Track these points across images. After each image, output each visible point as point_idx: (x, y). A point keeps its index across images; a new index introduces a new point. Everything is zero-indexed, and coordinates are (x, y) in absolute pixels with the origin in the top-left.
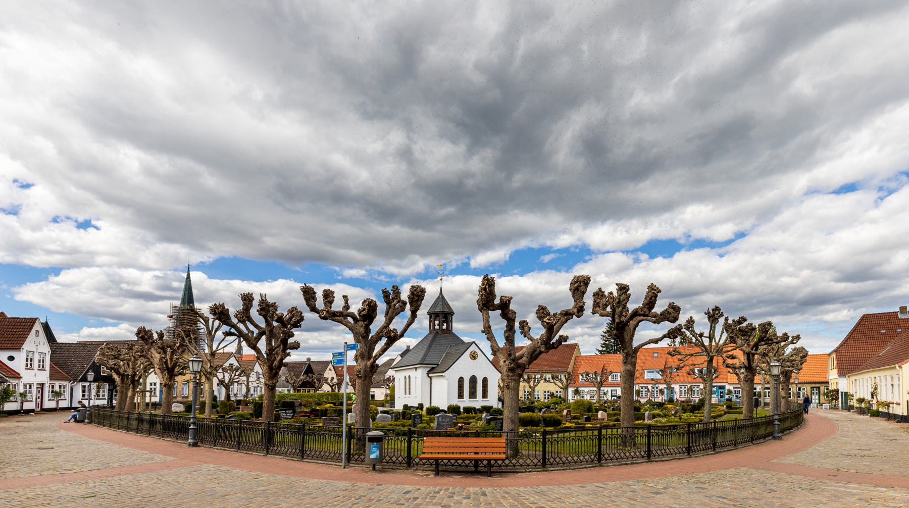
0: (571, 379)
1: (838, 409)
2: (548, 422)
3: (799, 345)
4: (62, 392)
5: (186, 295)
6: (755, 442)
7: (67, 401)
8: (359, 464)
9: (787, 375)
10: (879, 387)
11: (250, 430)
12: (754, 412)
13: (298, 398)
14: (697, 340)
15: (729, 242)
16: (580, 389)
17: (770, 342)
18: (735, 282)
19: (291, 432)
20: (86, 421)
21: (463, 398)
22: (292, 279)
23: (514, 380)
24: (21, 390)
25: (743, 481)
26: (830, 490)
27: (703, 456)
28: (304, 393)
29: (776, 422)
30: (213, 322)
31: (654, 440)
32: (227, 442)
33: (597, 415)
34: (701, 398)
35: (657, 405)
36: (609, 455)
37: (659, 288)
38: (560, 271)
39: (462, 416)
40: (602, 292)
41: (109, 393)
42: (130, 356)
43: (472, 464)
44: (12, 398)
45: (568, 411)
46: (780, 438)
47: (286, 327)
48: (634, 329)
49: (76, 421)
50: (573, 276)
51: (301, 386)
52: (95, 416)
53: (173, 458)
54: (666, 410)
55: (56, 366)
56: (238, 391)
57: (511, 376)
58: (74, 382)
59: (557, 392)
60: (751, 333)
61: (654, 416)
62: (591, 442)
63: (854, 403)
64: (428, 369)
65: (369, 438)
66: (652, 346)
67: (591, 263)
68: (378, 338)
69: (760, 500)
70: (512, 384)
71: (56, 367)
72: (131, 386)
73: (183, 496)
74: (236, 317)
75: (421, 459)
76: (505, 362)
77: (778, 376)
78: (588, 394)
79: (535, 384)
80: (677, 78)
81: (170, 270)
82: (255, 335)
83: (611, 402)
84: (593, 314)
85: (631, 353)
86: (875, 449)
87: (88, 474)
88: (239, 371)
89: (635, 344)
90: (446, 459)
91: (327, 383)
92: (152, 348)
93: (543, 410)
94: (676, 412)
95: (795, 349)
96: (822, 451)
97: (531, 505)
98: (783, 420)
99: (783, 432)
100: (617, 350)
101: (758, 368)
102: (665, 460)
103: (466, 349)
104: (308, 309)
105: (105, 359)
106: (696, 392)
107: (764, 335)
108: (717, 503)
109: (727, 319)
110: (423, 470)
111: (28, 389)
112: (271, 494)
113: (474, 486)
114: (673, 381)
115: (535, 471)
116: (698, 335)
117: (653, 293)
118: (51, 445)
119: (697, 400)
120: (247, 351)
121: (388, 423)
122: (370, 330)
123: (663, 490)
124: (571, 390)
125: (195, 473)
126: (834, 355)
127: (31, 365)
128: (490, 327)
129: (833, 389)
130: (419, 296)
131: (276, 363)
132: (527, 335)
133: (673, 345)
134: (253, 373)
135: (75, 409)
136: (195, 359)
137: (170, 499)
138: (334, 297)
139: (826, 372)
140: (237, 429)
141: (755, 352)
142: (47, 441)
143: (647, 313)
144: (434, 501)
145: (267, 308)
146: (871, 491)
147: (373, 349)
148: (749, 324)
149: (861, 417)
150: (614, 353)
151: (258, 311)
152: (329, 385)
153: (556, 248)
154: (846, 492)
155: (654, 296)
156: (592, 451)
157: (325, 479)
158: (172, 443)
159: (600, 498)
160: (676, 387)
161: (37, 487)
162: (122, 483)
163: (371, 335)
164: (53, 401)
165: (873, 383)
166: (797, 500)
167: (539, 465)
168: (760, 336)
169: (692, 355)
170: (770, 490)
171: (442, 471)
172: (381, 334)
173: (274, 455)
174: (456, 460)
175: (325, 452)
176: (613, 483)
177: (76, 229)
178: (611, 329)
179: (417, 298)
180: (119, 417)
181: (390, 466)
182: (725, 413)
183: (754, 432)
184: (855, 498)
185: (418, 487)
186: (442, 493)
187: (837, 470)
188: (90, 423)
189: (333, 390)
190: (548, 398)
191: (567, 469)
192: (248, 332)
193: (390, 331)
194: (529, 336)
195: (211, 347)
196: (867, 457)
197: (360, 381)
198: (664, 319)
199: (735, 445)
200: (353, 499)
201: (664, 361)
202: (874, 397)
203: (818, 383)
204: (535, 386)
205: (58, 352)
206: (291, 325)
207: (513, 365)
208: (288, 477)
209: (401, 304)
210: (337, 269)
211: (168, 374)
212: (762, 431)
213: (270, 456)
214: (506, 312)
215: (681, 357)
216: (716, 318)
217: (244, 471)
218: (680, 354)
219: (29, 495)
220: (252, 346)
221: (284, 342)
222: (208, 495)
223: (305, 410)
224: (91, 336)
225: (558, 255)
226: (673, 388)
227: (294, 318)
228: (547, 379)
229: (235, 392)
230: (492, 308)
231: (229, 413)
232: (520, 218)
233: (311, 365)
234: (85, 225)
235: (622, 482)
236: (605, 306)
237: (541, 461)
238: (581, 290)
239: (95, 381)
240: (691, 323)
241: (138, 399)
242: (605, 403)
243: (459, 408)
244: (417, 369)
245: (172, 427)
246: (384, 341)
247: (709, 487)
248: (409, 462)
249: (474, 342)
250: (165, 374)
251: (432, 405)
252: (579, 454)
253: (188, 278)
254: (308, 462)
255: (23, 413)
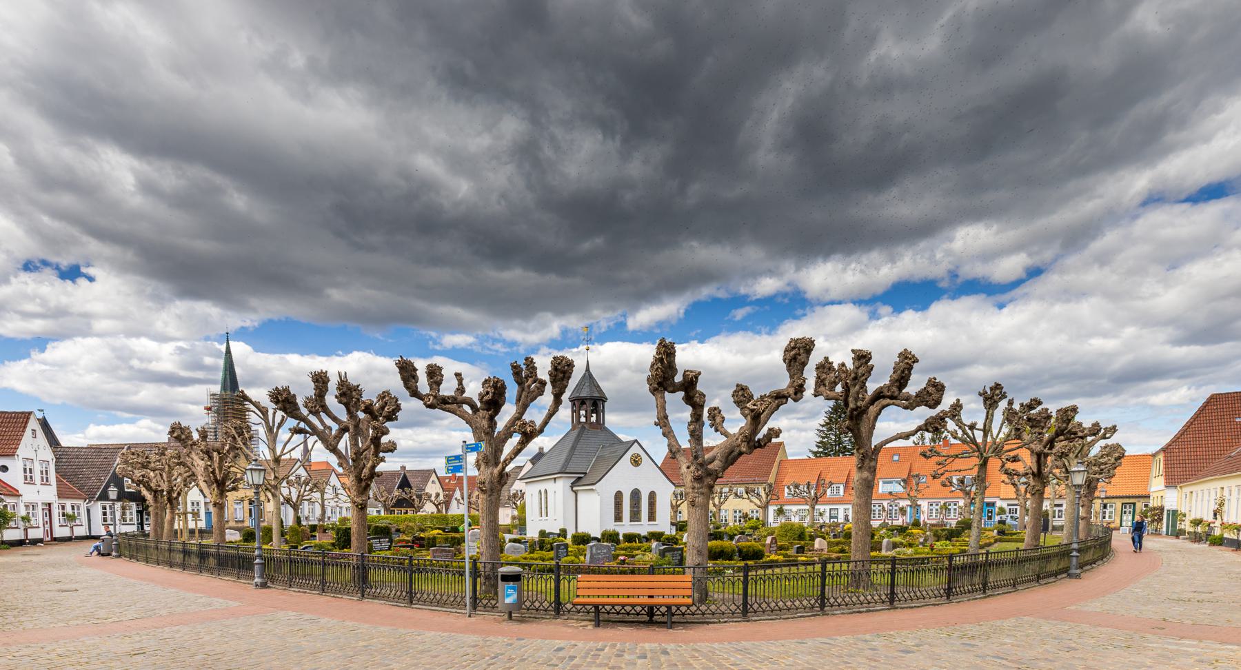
0: (772, 492)
1: (1161, 534)
2: (745, 555)
3: (1114, 440)
4: (76, 515)
5: (228, 376)
6: (1042, 581)
7: (84, 528)
8: (488, 611)
9: (1091, 486)
10: (1226, 503)
11: (337, 565)
12: (1042, 540)
13: (392, 522)
14: (964, 432)
15: (1017, 284)
16: (785, 508)
17: (1072, 436)
18: (1020, 345)
19: (393, 567)
20: (114, 553)
21: (655, 521)
22: (372, 351)
23: (702, 494)
24: (23, 512)
25: (1028, 636)
26: (1156, 648)
27: (968, 600)
28: (400, 515)
29: (1074, 553)
30: (274, 413)
31: (900, 579)
32: (307, 582)
33: (814, 544)
34: (960, 519)
35: (897, 529)
36: (836, 599)
37: (916, 356)
38: (759, 333)
39: (622, 545)
40: (830, 363)
41: (138, 516)
42: (162, 465)
43: (645, 611)
44: (12, 524)
45: (773, 539)
46: (1078, 576)
47: (378, 421)
48: (876, 418)
49: (100, 554)
50: (789, 340)
51: (395, 506)
52: (125, 547)
53: (238, 604)
54: (910, 536)
55: (64, 479)
56: (309, 512)
57: (698, 489)
58: (90, 501)
59: (752, 512)
60: (1045, 423)
61: (895, 546)
62: (811, 581)
63: (1187, 526)
64: (573, 480)
65: (502, 576)
66: (900, 443)
67: (805, 319)
68: (508, 434)
69: (1054, 661)
70: (699, 500)
71: (65, 481)
72: (168, 505)
73: (261, 653)
74: (306, 406)
75: (574, 605)
76: (688, 467)
77: (1079, 486)
78: (797, 514)
79: (722, 500)
80: (948, 15)
81: (199, 340)
82: (334, 432)
83: (830, 527)
84: (816, 396)
85: (870, 454)
86: (1218, 591)
87: (129, 624)
88: (310, 484)
89: (875, 442)
90: (609, 605)
91: (431, 501)
92: (193, 453)
93: (737, 537)
94: (926, 540)
95: (1105, 447)
96: (1140, 593)
97: (732, 667)
98: (1083, 550)
99: (1082, 568)
100: (839, 451)
101: (1051, 475)
102: (915, 607)
103: (624, 451)
104: (408, 393)
105: (129, 469)
106: (952, 511)
107: (1064, 425)
108: (993, 665)
109: (1011, 403)
110: (577, 620)
111: (31, 511)
112: (376, 651)
113: (650, 641)
114: (919, 496)
115: (733, 622)
116: (968, 426)
117: (907, 363)
118: (74, 586)
119: (954, 523)
120: (320, 454)
121: (521, 555)
122: (496, 424)
123: (915, 648)
124: (772, 509)
125: (270, 623)
126: (1161, 456)
127: (31, 477)
128: (666, 417)
129: (1156, 505)
130: (564, 372)
131: (366, 471)
132: (719, 428)
133: (921, 443)
134: (328, 487)
135: (97, 538)
136: (254, 467)
137: (244, 658)
138: (442, 376)
139: (1146, 480)
140: (320, 564)
141: (1049, 451)
142: (67, 581)
143: (896, 393)
144: (598, 661)
145: (348, 393)
146: (1215, 649)
147: (501, 451)
148: (1042, 409)
149: (1196, 545)
150: (834, 455)
151: (336, 397)
152: (434, 503)
153: (754, 298)
154: (1178, 650)
155: (908, 369)
156: (811, 594)
157: (445, 631)
158: (233, 583)
159: (827, 658)
160: (924, 504)
161: (68, 641)
162: (177, 636)
163: (497, 430)
164: (15, 530)
165: (1218, 496)
166: (1109, 662)
167: (738, 613)
168: (1059, 427)
169: (957, 456)
170: (1068, 648)
171: (603, 621)
172: (512, 429)
173: (371, 599)
174: (623, 606)
175: (442, 596)
176: (843, 638)
177: (59, 280)
178: (831, 420)
179: (561, 375)
180: (157, 548)
181: (532, 614)
182: (996, 541)
183: (1042, 568)
184: (1193, 660)
185: (573, 642)
186: (607, 649)
187: (1164, 620)
188: (119, 556)
189: (439, 511)
190: (740, 521)
191: (777, 619)
192: (324, 427)
193: (525, 424)
194: (722, 430)
195: (273, 450)
196: (1207, 603)
197: (485, 496)
198: (921, 403)
199: (1014, 586)
200: (487, 658)
201: (908, 467)
202: (1218, 516)
203: (1133, 497)
204: (721, 503)
205: (64, 460)
206: (384, 417)
207: (700, 472)
208: (395, 628)
209: (538, 385)
210: (434, 334)
211: (218, 489)
212: (1053, 566)
213: (367, 600)
214: (691, 394)
215: (941, 459)
216: (995, 402)
217: (335, 621)
218: (938, 454)
219: (59, 651)
220: (331, 448)
221: (376, 441)
222: (293, 653)
223: (406, 538)
224: (101, 437)
225: (757, 308)
226: (920, 506)
227: (387, 407)
228: (738, 494)
229: (306, 514)
230: (671, 389)
231: (302, 543)
232: (701, 253)
233: (407, 475)
234: (72, 274)
235: (855, 636)
236: (833, 385)
237: (741, 607)
238: (800, 360)
239: (119, 499)
240: (958, 409)
241: (179, 524)
242: (821, 527)
243: (617, 534)
244: (557, 480)
245: (230, 563)
246: (516, 439)
247: (980, 644)
248: (558, 608)
249: (636, 441)
250: (214, 489)
251: (580, 530)
252: (792, 598)
253: (228, 352)
254: (419, 609)
255: (29, 544)
